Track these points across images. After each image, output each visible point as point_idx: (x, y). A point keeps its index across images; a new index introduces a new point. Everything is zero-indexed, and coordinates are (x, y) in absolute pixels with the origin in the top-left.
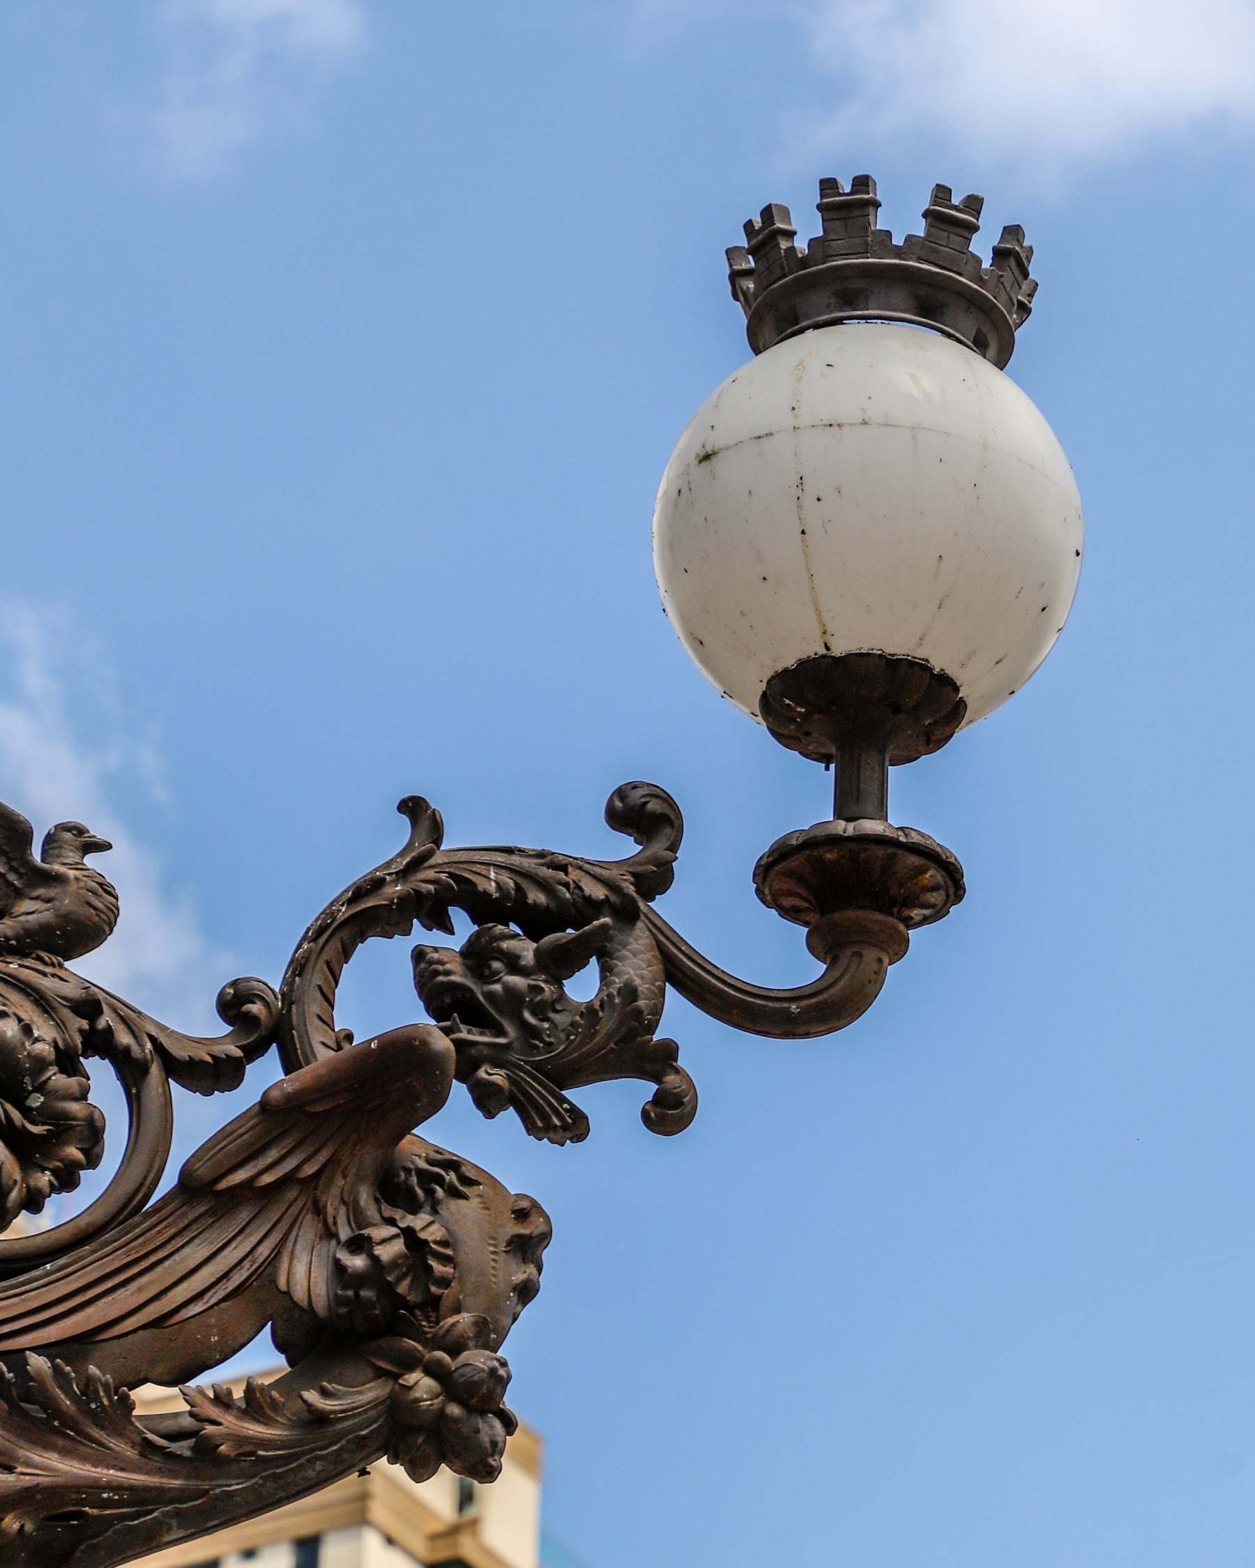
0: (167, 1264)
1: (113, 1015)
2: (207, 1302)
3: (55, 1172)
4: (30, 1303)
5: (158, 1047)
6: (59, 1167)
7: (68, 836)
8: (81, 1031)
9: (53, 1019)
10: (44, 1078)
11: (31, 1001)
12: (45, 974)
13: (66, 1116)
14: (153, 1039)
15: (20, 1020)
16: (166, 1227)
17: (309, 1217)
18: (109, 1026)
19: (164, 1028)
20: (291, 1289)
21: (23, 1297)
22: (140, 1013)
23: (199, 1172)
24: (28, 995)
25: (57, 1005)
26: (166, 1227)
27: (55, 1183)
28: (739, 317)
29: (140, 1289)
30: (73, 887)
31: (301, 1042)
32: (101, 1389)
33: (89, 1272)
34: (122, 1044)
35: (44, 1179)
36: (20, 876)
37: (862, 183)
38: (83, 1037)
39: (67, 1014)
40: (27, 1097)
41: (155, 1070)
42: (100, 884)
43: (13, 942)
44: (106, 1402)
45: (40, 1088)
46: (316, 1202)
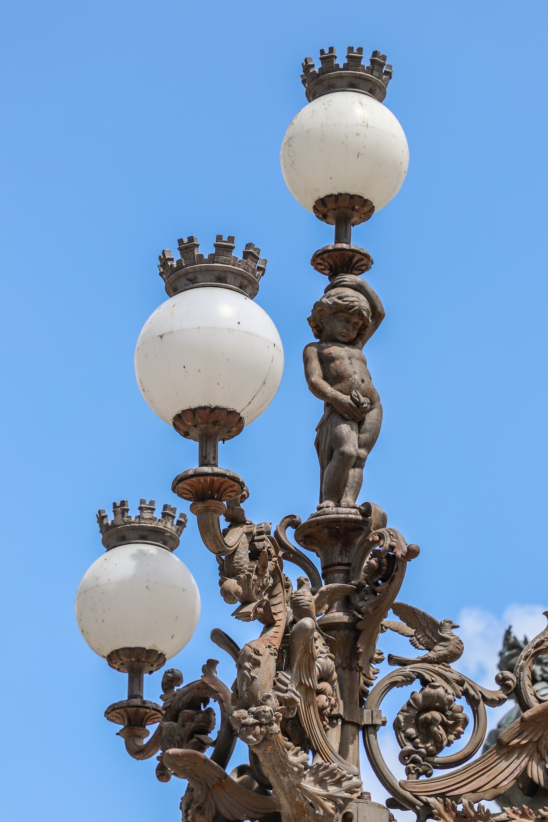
0: (495, 768)
1: (468, 684)
2: (509, 781)
3: (455, 735)
4: (457, 780)
5: (483, 696)
6: (456, 734)
7: (447, 624)
8: (461, 691)
9: (451, 686)
10: (452, 706)
11: (443, 679)
12: (446, 671)
13: (458, 718)
14: (481, 692)
15: (444, 688)
16: (494, 756)
17: (536, 753)
18: (467, 688)
19: (482, 688)
20: (533, 777)
21: (454, 778)
22: (475, 683)
23: (504, 740)
24: (442, 678)
25: (452, 681)
26: (494, 756)
27: (455, 738)
28: (162, 284)
29: (488, 776)
30: (452, 642)
31: (524, 693)
32: (482, 809)
33: (473, 771)
34: (472, 694)
35: (452, 737)
36: (436, 638)
37: (191, 239)
38: (462, 693)
39: (455, 685)
40: (446, 712)
41: (481, 702)
42: (460, 641)
43: (436, 660)
44: (483, 813)
45: (450, 709)
46: (538, 749)
